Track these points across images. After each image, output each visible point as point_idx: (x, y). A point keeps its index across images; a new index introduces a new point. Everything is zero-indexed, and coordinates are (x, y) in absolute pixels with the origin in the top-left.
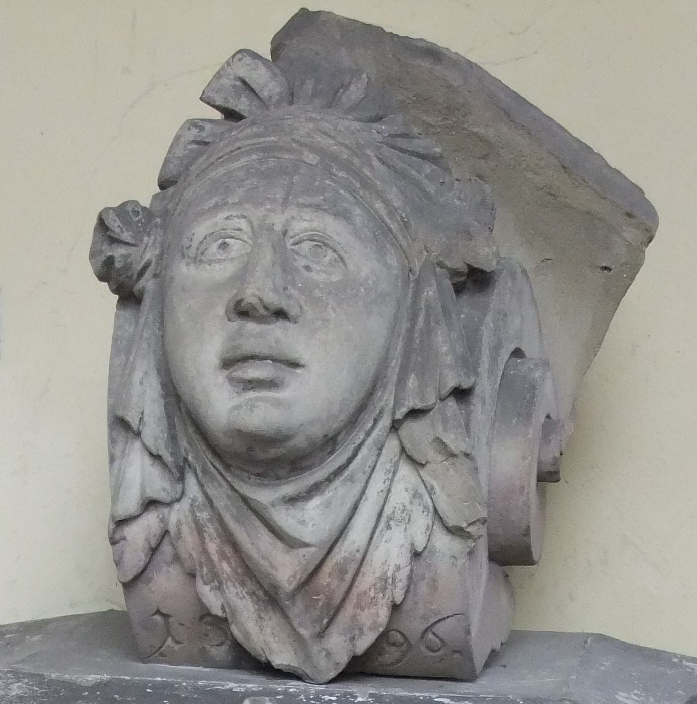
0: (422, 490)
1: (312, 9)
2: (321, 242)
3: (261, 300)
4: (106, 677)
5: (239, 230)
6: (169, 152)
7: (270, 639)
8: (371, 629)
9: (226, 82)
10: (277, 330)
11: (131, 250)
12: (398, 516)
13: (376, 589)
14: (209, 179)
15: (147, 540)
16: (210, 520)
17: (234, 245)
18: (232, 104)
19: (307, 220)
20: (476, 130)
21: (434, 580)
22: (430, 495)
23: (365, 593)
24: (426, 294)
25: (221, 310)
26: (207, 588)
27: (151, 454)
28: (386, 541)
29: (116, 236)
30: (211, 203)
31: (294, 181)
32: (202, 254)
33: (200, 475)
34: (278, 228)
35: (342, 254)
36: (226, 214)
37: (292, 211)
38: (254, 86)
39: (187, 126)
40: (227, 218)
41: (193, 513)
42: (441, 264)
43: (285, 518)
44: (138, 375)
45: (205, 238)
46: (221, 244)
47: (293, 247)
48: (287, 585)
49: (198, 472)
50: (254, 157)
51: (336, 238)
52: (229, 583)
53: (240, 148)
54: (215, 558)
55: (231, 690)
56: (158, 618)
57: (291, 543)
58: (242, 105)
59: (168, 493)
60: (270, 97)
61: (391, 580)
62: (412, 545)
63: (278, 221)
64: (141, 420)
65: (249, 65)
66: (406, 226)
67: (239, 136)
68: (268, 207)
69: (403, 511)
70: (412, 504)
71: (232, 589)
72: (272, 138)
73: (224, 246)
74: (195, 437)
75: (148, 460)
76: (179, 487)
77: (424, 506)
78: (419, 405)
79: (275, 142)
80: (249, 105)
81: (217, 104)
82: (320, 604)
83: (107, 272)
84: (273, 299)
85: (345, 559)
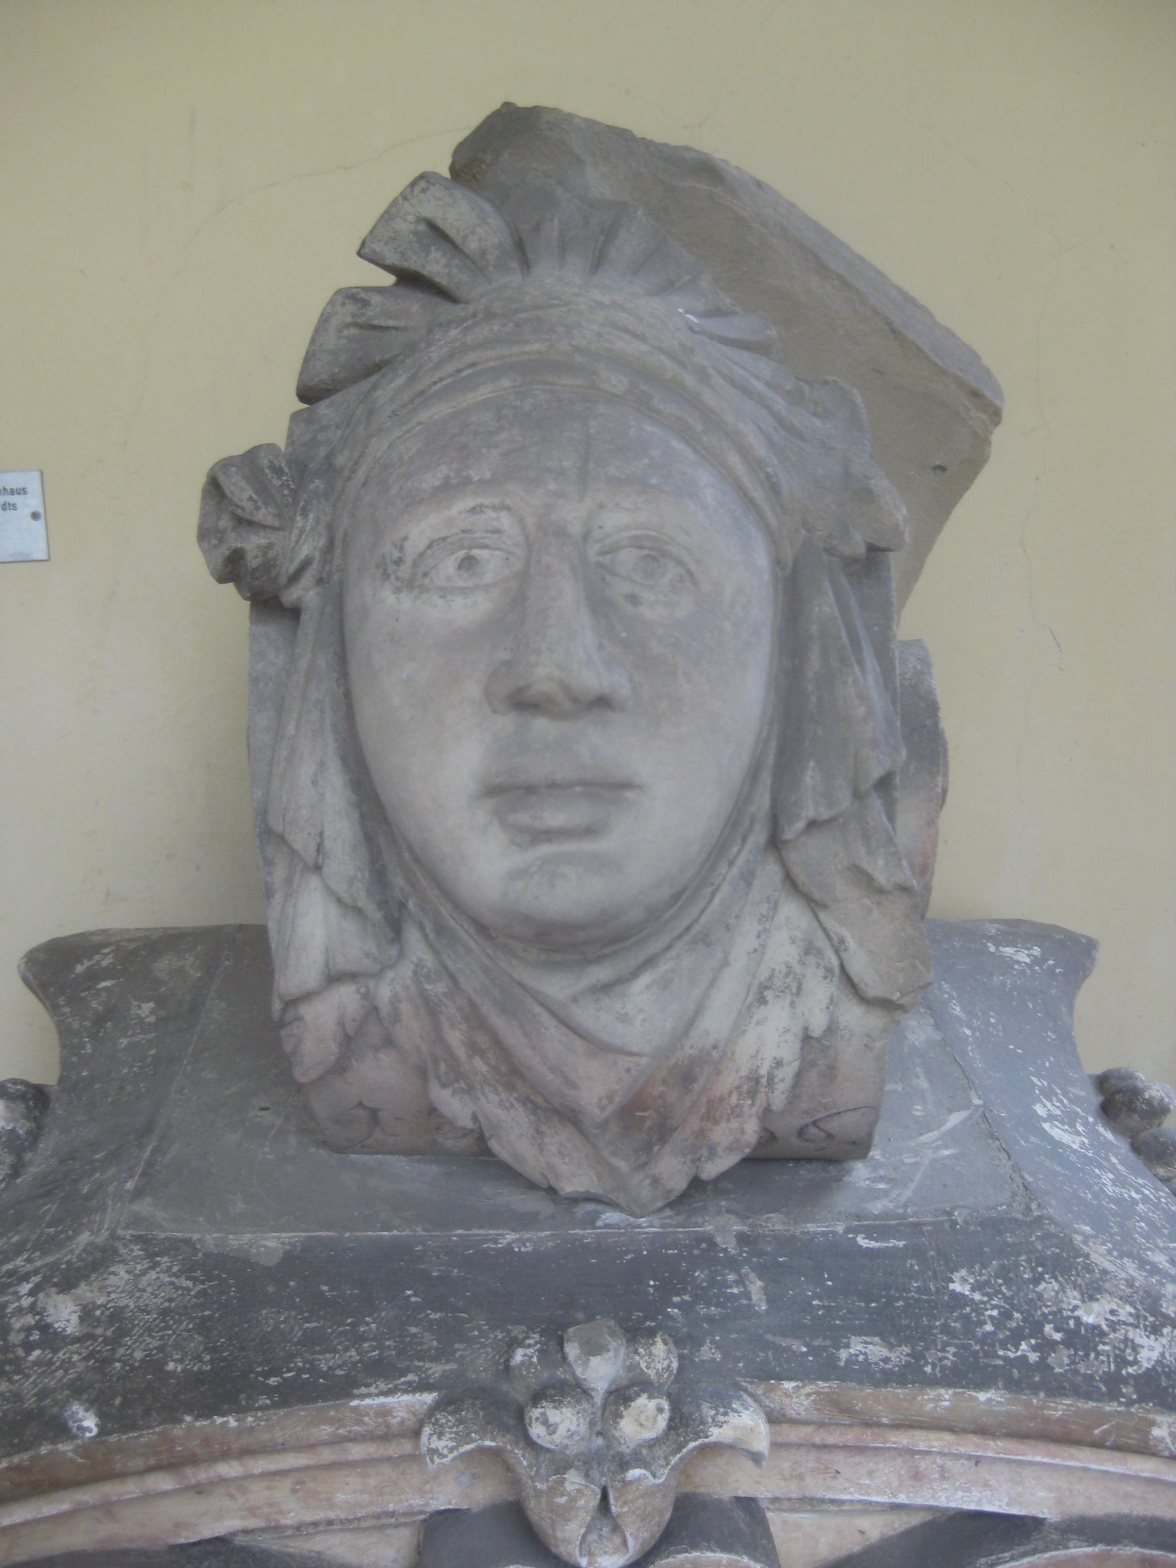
0: (821, 942)
5: (497, 531)
6: (313, 341)
7: (557, 1161)
8: (730, 1149)
9: (404, 227)
11: (274, 537)
12: (778, 982)
13: (740, 1094)
14: (419, 423)
15: (341, 1023)
17: (488, 561)
18: (414, 263)
19: (628, 509)
21: (832, 1068)
22: (837, 952)
23: (721, 1099)
24: (817, 609)
25: (473, 690)
26: (447, 1093)
27: (339, 901)
28: (757, 1023)
29: (247, 516)
30: (431, 480)
31: (592, 431)
32: (425, 575)
33: (431, 936)
34: (576, 529)
35: (693, 567)
36: (470, 502)
38: (451, 232)
39: (339, 299)
40: (473, 511)
42: (830, 551)
43: (590, 1016)
44: (306, 770)
45: (429, 547)
46: (463, 560)
47: (600, 559)
48: (597, 1111)
49: (428, 931)
50: (506, 383)
52: (487, 1089)
53: (473, 365)
54: (461, 1052)
55: (508, 1249)
57: (599, 1047)
58: (435, 265)
59: (375, 959)
60: (483, 253)
61: (765, 1080)
62: (806, 1029)
63: (571, 514)
64: (320, 848)
65: (440, 199)
67: (469, 339)
68: (552, 486)
69: (787, 975)
70: (804, 964)
71: (491, 1096)
73: (468, 563)
75: (334, 910)
76: (393, 952)
77: (825, 968)
78: (825, 813)
79: (539, 352)
80: (446, 266)
81: (388, 262)
82: (648, 1124)
83: (232, 569)
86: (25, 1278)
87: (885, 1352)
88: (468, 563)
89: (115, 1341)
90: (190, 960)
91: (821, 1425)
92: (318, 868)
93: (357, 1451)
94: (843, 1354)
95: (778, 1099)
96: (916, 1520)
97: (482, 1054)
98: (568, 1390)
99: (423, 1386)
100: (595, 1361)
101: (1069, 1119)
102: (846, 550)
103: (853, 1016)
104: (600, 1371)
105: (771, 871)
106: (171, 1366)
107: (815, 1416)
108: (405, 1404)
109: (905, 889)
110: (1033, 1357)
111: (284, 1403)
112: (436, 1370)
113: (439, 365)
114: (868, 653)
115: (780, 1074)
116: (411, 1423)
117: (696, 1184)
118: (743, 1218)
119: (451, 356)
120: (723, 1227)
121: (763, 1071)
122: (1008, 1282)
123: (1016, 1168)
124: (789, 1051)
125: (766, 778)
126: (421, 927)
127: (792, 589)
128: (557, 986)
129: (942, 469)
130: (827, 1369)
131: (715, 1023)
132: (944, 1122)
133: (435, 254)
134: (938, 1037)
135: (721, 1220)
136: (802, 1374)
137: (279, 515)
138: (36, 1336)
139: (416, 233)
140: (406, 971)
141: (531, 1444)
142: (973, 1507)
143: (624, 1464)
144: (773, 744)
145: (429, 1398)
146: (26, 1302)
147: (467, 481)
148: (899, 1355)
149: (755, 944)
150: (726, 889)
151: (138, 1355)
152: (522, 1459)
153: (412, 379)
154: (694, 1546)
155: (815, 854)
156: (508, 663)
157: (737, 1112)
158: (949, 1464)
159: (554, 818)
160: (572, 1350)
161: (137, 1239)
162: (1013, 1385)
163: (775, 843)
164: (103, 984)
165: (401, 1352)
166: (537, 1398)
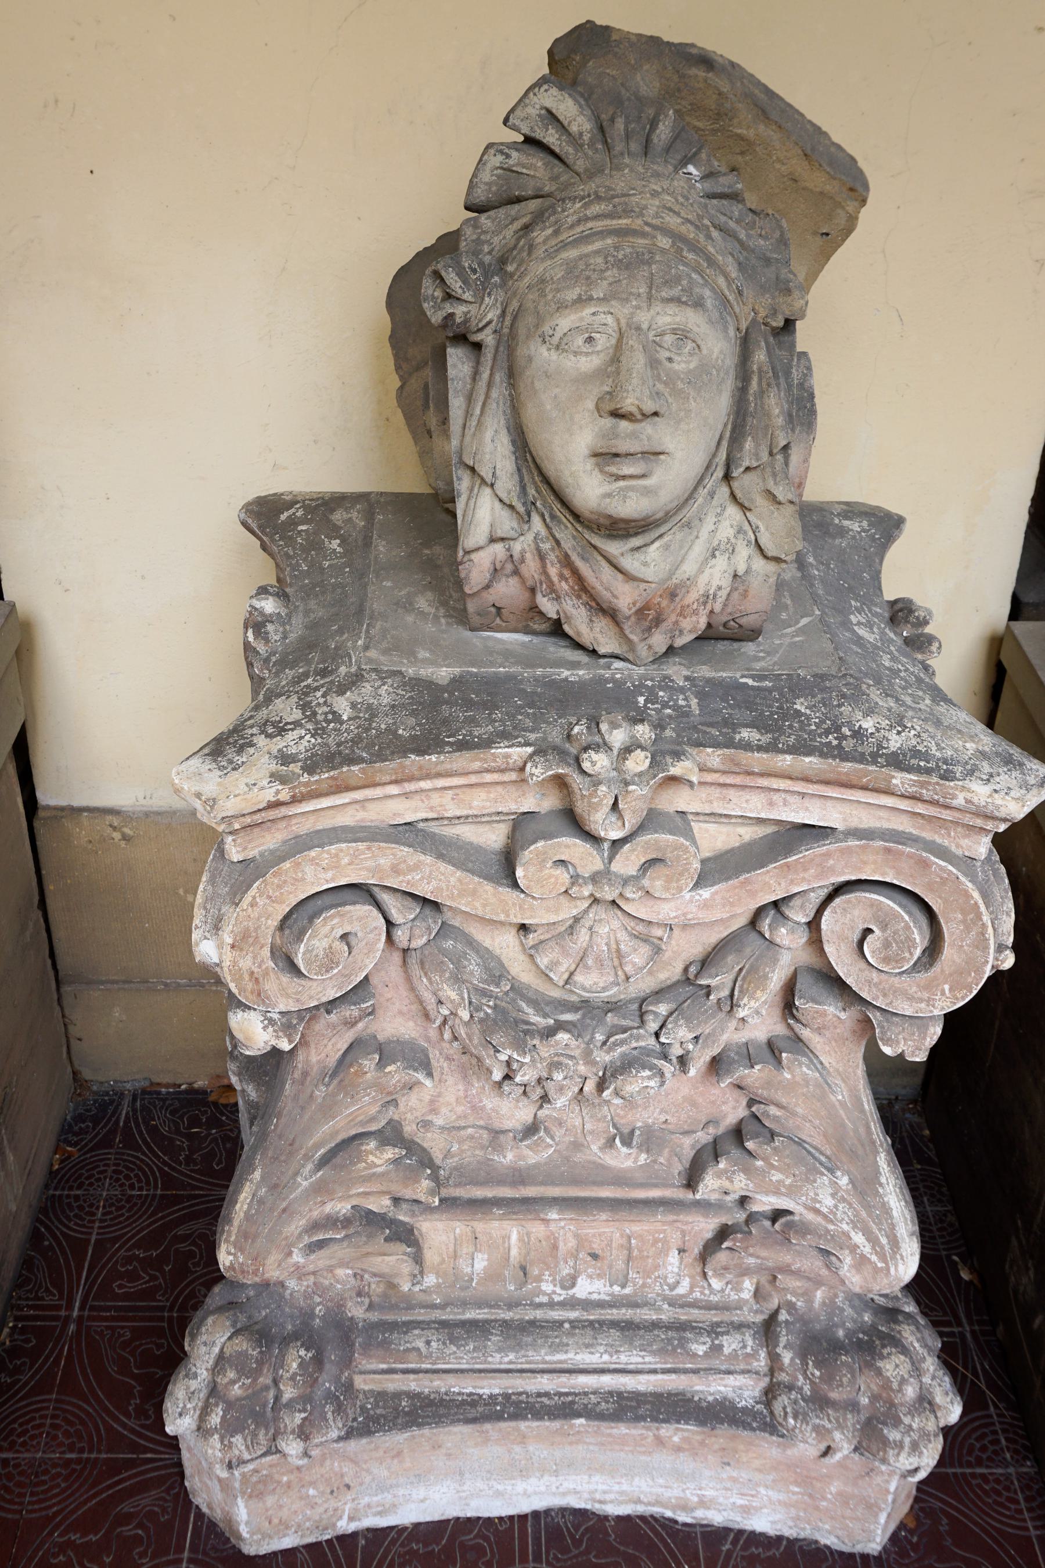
0: (747, 527)
1: (599, 22)
2: (682, 335)
3: (640, 410)
4: (457, 670)
7: (599, 636)
10: (647, 428)
11: (471, 307)
12: (722, 547)
16: (553, 549)
18: (539, 134)
20: (739, 131)
21: (746, 591)
25: (590, 405)
27: (501, 501)
36: (593, 310)
37: (658, 307)
38: (561, 118)
40: (594, 314)
41: (537, 544)
42: (765, 324)
43: (629, 563)
44: (489, 434)
50: (609, 241)
51: (695, 329)
55: (566, 680)
56: (493, 609)
58: (551, 137)
60: (581, 134)
63: (643, 318)
66: (740, 293)
67: (588, 212)
72: (625, 221)
73: (590, 340)
74: (543, 488)
84: (649, 406)
85: (676, 586)
86: (317, 689)
87: (758, 737)
88: (590, 340)
89: (370, 720)
90: (354, 514)
91: (724, 772)
92: (492, 485)
93: (488, 778)
94: (738, 737)
95: (718, 608)
96: (770, 830)
97: (566, 580)
98: (604, 746)
99: (527, 744)
100: (615, 732)
101: (869, 625)
102: (774, 324)
103: (759, 564)
104: (618, 737)
105: (724, 490)
106: (400, 732)
107: (722, 767)
108: (518, 753)
109: (791, 502)
110: (835, 742)
111: (459, 750)
112: (532, 737)
113: (572, 227)
114: (782, 380)
115: (719, 593)
116: (520, 763)
117: (671, 650)
118: (688, 668)
119: (579, 221)
120: (677, 671)
121: (711, 592)
122: (824, 705)
123: (836, 649)
124: (726, 582)
125: (725, 444)
126: (543, 516)
127: (745, 345)
128: (613, 548)
129: (827, 234)
130: (730, 744)
131: (689, 568)
132: (797, 622)
133: (551, 131)
134: (799, 574)
135: (676, 668)
136: (716, 745)
137: (474, 296)
138: (330, 717)
139: (540, 116)
140: (530, 537)
141: (583, 772)
142: (800, 821)
143: (627, 784)
144: (729, 426)
145: (530, 750)
146: (322, 700)
147: (591, 299)
148: (766, 739)
149: (713, 528)
150: (700, 500)
151: (383, 726)
152: (576, 780)
153: (556, 233)
154: (656, 832)
155: (747, 484)
156: (608, 393)
157: (695, 612)
158: (788, 797)
159: (627, 470)
160: (604, 727)
161: (375, 670)
162: (823, 755)
163: (727, 477)
164: (300, 528)
165: (515, 728)
166: (586, 749)
